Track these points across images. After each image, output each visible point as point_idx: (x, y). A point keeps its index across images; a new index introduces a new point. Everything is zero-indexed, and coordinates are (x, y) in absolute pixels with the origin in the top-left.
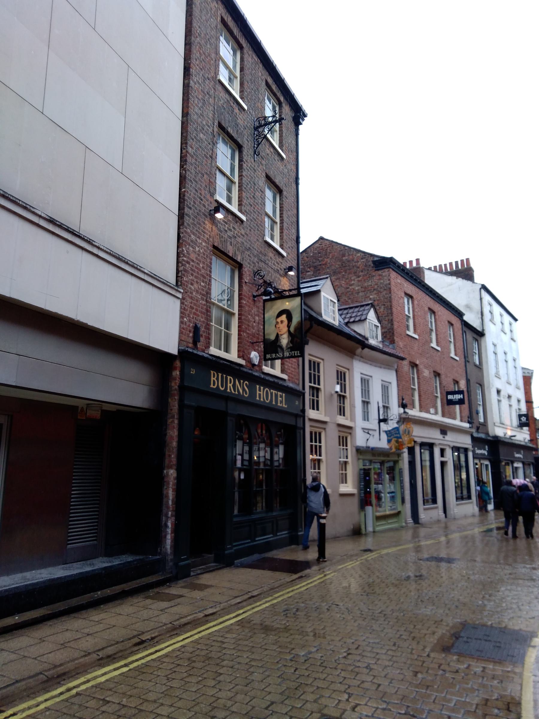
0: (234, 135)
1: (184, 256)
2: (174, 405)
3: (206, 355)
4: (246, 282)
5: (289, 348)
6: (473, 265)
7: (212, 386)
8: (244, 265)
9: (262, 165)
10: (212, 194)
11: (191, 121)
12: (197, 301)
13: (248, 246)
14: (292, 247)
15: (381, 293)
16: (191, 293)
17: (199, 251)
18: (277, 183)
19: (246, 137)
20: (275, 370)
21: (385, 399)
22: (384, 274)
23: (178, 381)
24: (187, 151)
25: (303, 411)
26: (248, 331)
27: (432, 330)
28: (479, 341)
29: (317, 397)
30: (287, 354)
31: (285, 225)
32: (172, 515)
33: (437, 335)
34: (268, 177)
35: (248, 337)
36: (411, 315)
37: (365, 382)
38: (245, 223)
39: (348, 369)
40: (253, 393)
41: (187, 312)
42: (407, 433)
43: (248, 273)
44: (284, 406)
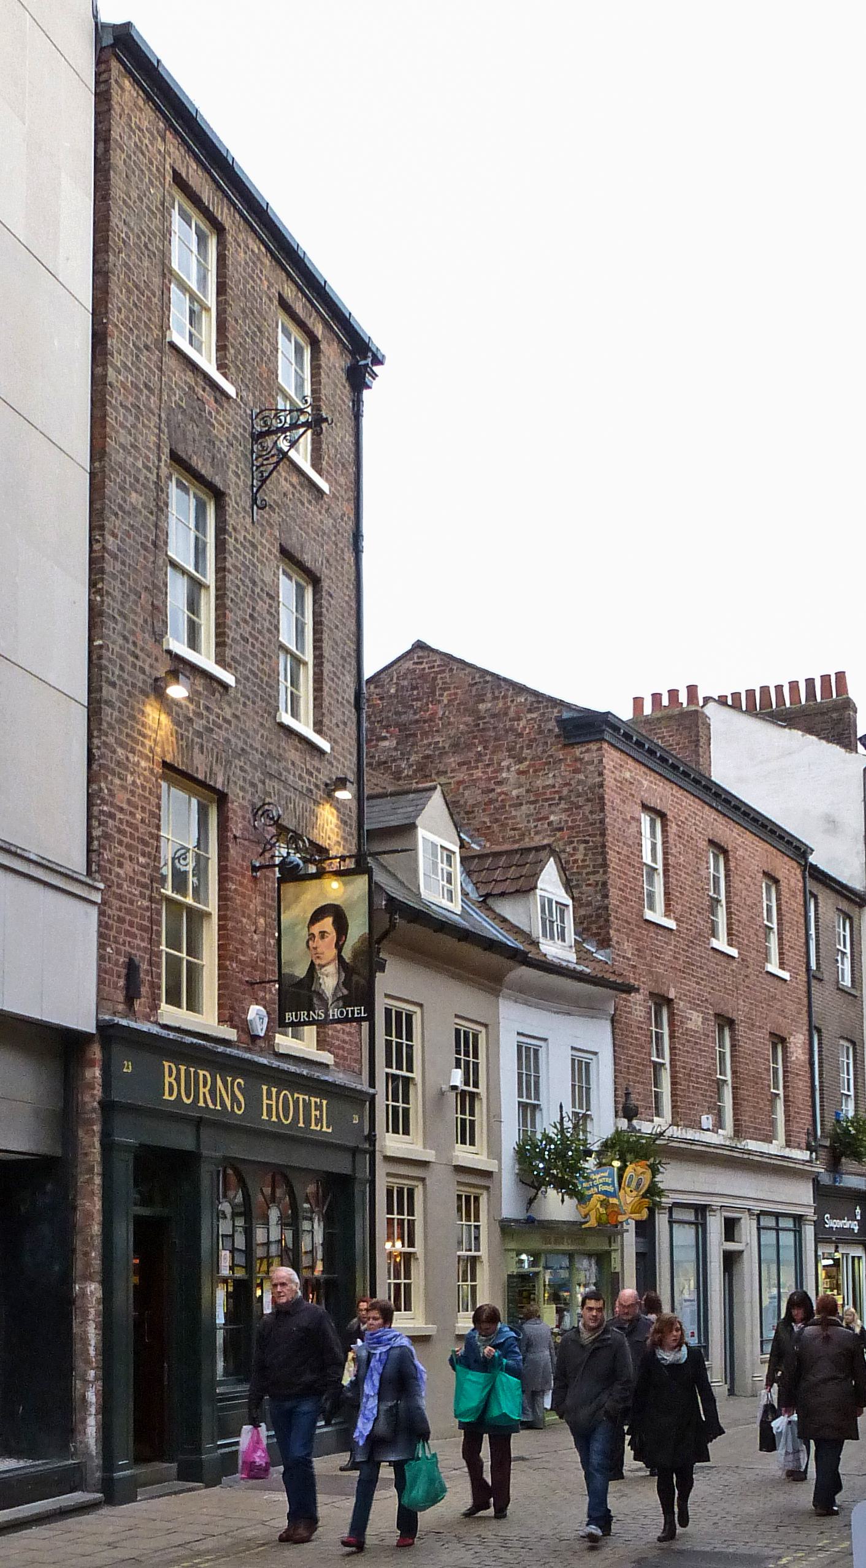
0: (205, 471)
1: (104, 801)
2: (92, 1145)
3: (155, 1030)
4: (235, 837)
5: (338, 999)
6: (854, 692)
7: (166, 1097)
8: (231, 796)
9: (271, 526)
10: (158, 637)
11: (112, 469)
12: (132, 902)
13: (240, 744)
14: (345, 724)
15: (579, 807)
16: (120, 886)
17: (134, 782)
18: (308, 564)
19: (233, 467)
20: (302, 1044)
21: (581, 1099)
22: (587, 757)
23: (98, 1092)
24: (104, 547)
25: (371, 1138)
26: (243, 958)
27: (718, 901)
28: (855, 920)
29: (406, 1100)
30: (334, 1013)
31: (327, 667)
32: (96, 1379)
33: (729, 914)
34: (285, 553)
35: (242, 971)
36: (660, 866)
37: (529, 1056)
38: (232, 692)
39: (486, 1026)
40: (254, 1102)
41: (113, 933)
42: (634, 1184)
43: (240, 813)
44: (325, 1129)
